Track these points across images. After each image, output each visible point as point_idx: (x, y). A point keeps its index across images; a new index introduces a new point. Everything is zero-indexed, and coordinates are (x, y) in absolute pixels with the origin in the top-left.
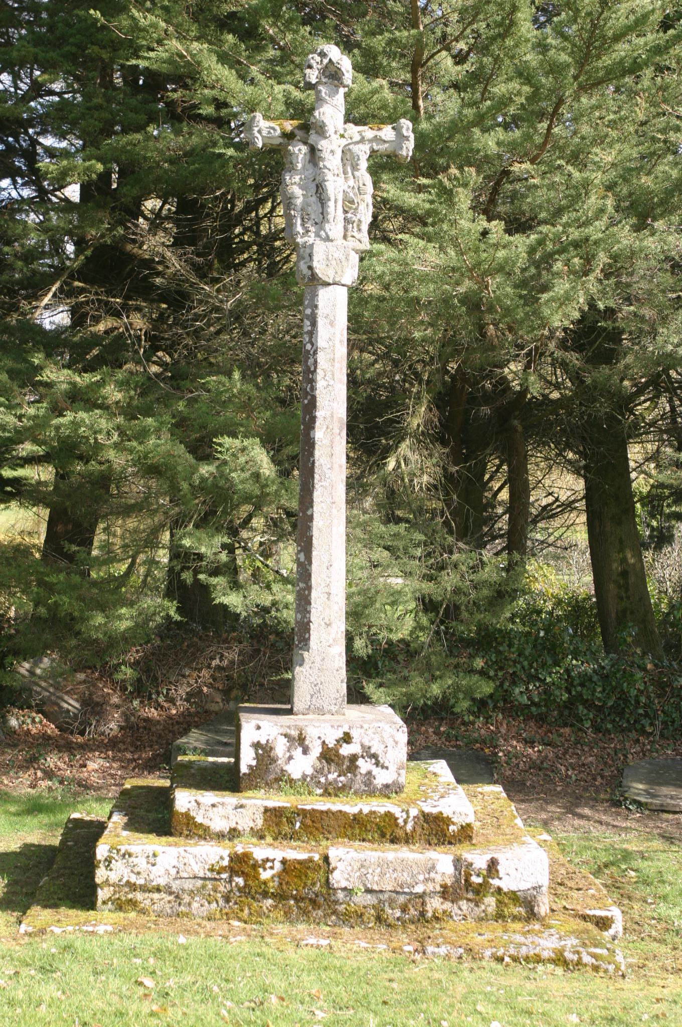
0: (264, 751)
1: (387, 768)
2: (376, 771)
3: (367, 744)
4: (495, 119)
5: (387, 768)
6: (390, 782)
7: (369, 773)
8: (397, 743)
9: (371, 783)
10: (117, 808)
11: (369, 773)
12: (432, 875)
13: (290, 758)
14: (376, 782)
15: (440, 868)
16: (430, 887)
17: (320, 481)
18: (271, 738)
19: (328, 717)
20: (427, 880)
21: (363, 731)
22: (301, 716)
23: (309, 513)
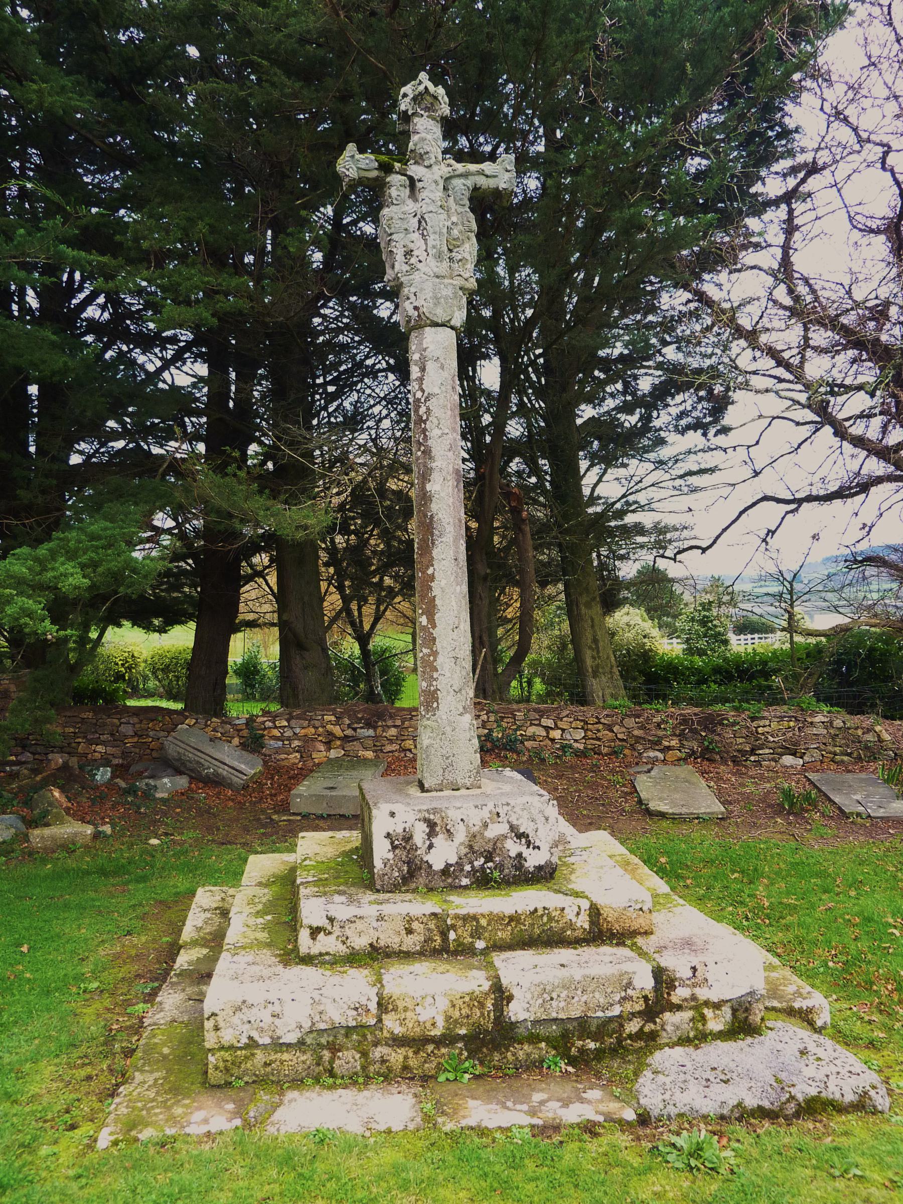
0: (402, 842)
1: (538, 848)
2: (526, 852)
3: (515, 822)
4: (347, 310)
5: (538, 848)
6: (542, 863)
7: (520, 855)
8: (547, 819)
9: (522, 866)
10: (117, 287)
11: (520, 855)
12: (629, 992)
13: (431, 846)
14: (527, 865)
15: (638, 983)
16: (628, 1007)
17: (440, 537)
18: (407, 826)
19: (463, 792)
20: (624, 999)
21: (509, 808)
22: (434, 794)
23: (430, 571)
